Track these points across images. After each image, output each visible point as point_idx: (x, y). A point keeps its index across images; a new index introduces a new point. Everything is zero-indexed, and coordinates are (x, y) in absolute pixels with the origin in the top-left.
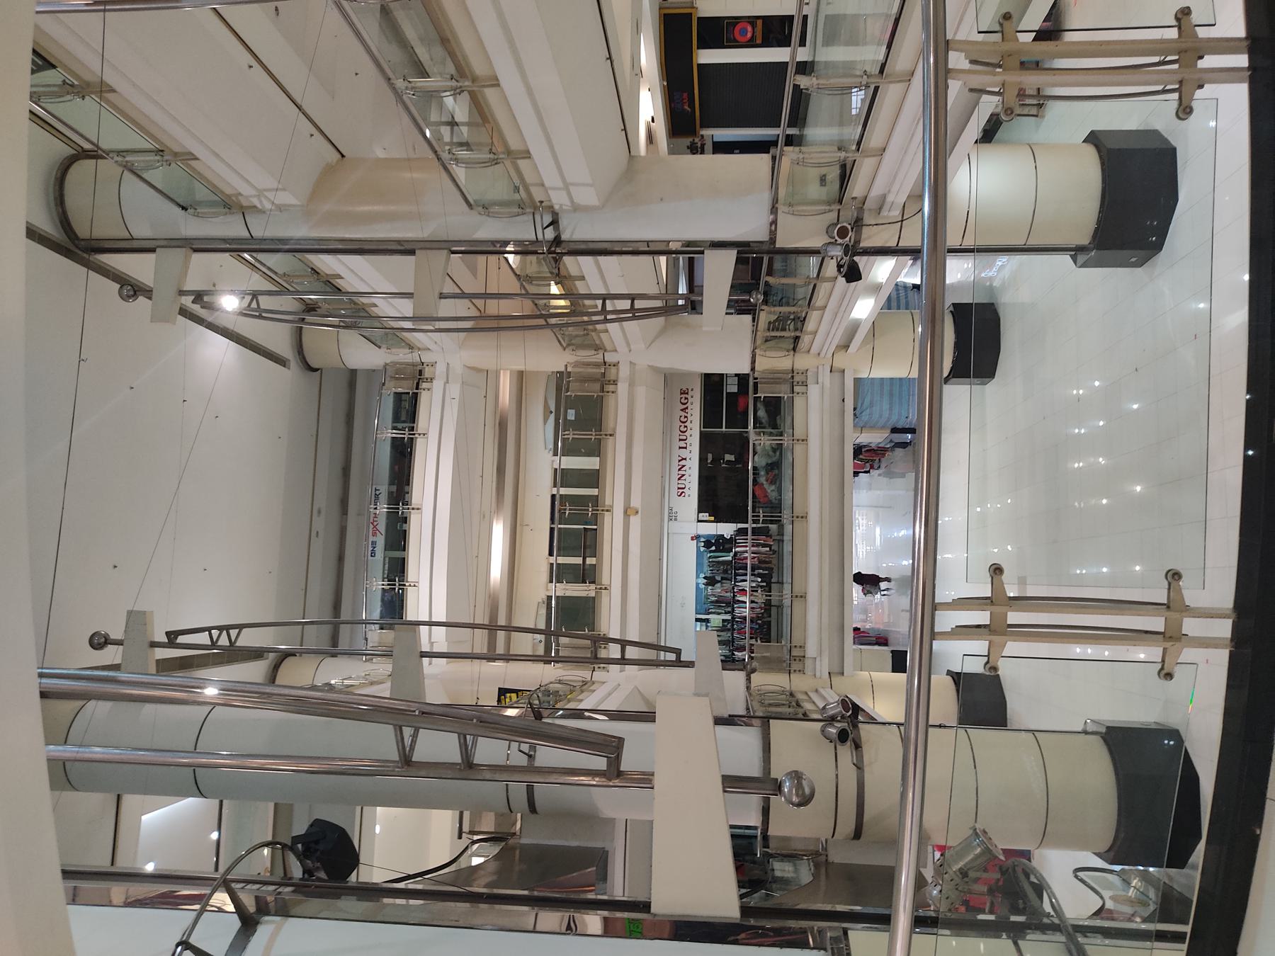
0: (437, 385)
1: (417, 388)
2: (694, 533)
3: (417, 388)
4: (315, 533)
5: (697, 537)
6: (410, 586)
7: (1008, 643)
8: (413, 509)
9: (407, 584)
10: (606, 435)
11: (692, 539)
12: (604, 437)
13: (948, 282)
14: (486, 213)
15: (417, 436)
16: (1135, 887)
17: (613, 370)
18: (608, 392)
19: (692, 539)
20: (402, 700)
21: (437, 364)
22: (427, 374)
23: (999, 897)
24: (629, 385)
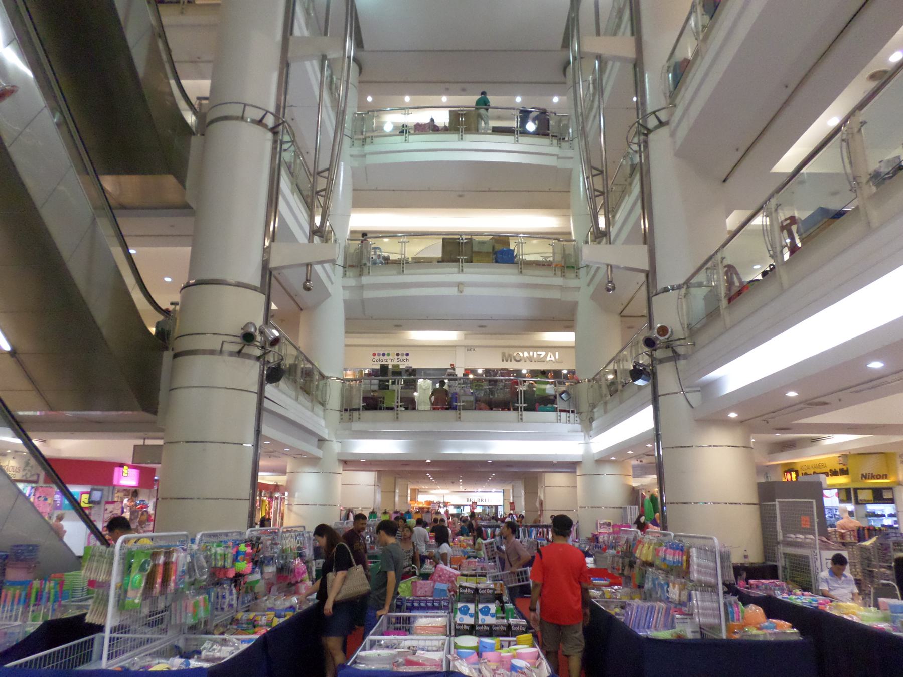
0: (555, 150)
1: (553, 136)
2: (456, 365)
3: (553, 136)
4: (485, 325)
5: (453, 368)
6: (406, 137)
7: (264, 296)
8: (462, 136)
9: (407, 135)
10: (521, 268)
11: (452, 365)
12: (520, 267)
13: (651, 406)
14: (680, 297)
15: (516, 136)
16: (106, 558)
17: (573, 275)
18: (555, 270)
19: (452, 365)
20: (319, 109)
21: (578, 280)
22: (563, 144)
23: (178, 557)
24: (561, 286)
